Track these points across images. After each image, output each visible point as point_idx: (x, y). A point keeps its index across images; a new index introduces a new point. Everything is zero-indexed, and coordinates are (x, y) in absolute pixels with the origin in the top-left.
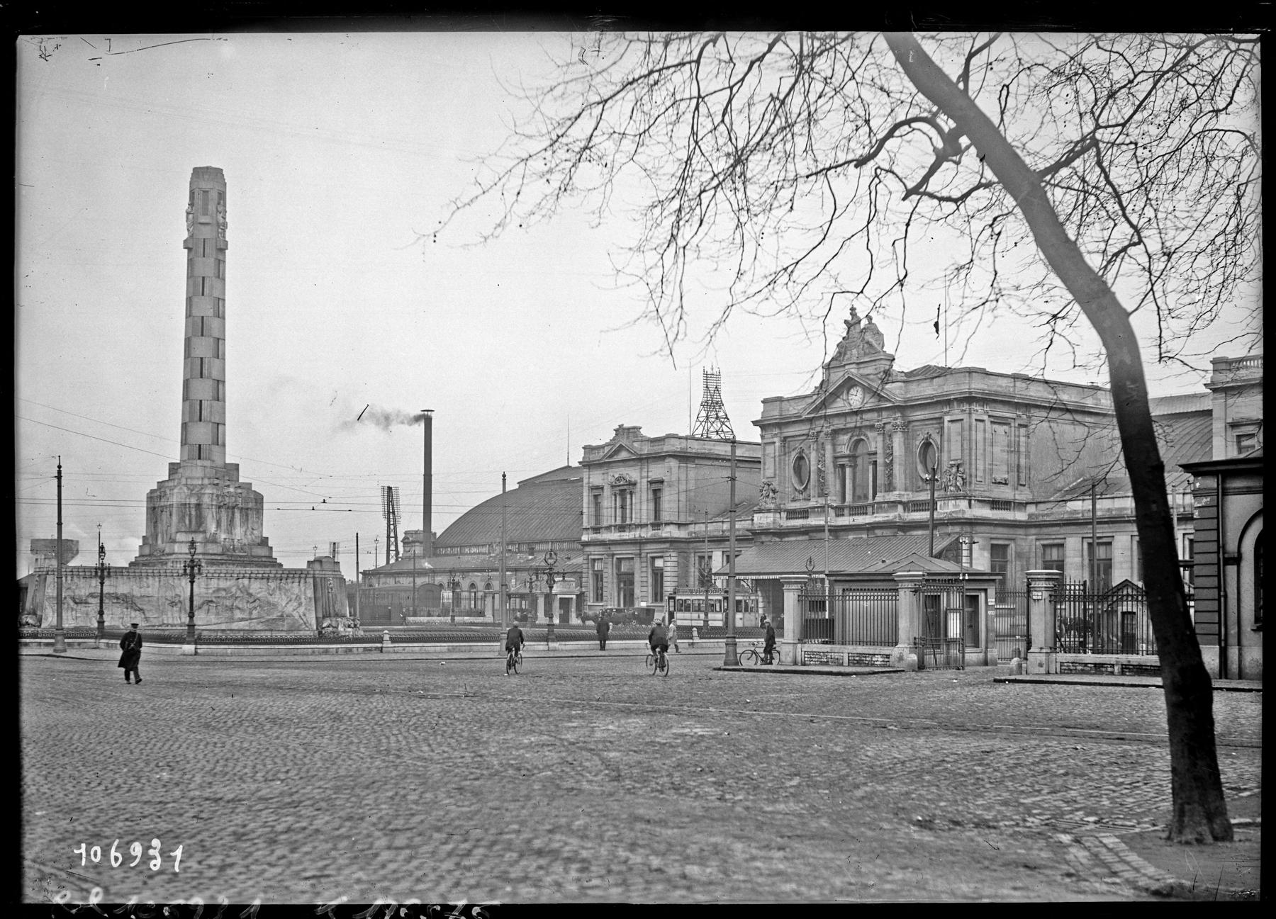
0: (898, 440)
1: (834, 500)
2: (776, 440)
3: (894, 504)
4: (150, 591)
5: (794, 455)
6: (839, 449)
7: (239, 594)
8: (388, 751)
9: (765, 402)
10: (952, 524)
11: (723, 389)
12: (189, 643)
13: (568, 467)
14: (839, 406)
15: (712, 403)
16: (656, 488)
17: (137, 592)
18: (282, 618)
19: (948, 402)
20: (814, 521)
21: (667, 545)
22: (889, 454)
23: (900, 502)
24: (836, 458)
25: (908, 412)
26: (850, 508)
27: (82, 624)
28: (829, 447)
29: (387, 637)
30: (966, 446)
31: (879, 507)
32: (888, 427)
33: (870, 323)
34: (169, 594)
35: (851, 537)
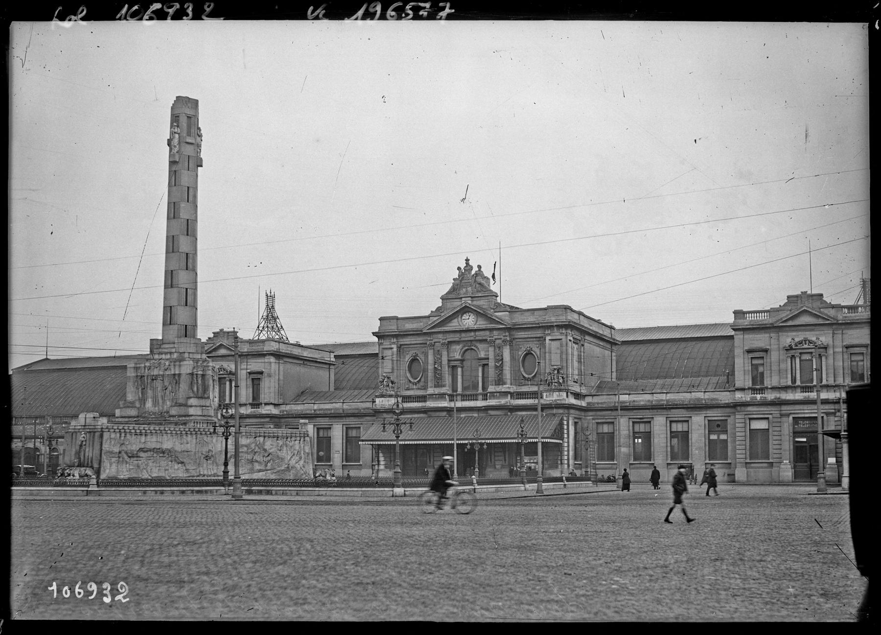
0: (506, 353)
1: (446, 390)
2: (394, 346)
3: (505, 394)
4: (188, 447)
5: (408, 358)
6: (451, 355)
7: (257, 449)
8: (345, 565)
9: (381, 319)
10: (556, 408)
11: (276, 307)
12: (398, 487)
13: (47, 359)
14: (454, 325)
15: (271, 317)
16: (256, 378)
17: (178, 448)
18: (288, 469)
19: (550, 327)
20: (431, 404)
21: (268, 420)
22: (500, 359)
23: (509, 393)
24: (449, 361)
25: (513, 333)
26: (462, 395)
27: (135, 475)
28: (445, 353)
29: (475, 481)
30: (564, 356)
31: (493, 395)
32: (498, 342)
33: (480, 270)
34: (205, 450)
35: (463, 416)
